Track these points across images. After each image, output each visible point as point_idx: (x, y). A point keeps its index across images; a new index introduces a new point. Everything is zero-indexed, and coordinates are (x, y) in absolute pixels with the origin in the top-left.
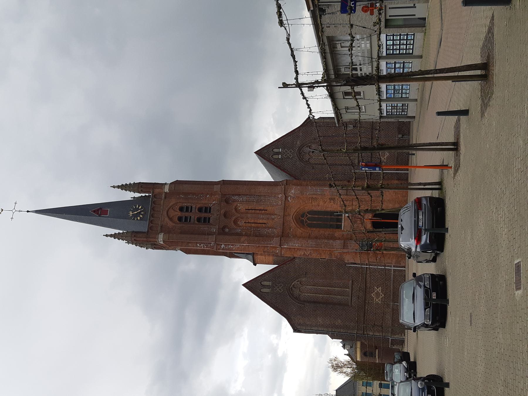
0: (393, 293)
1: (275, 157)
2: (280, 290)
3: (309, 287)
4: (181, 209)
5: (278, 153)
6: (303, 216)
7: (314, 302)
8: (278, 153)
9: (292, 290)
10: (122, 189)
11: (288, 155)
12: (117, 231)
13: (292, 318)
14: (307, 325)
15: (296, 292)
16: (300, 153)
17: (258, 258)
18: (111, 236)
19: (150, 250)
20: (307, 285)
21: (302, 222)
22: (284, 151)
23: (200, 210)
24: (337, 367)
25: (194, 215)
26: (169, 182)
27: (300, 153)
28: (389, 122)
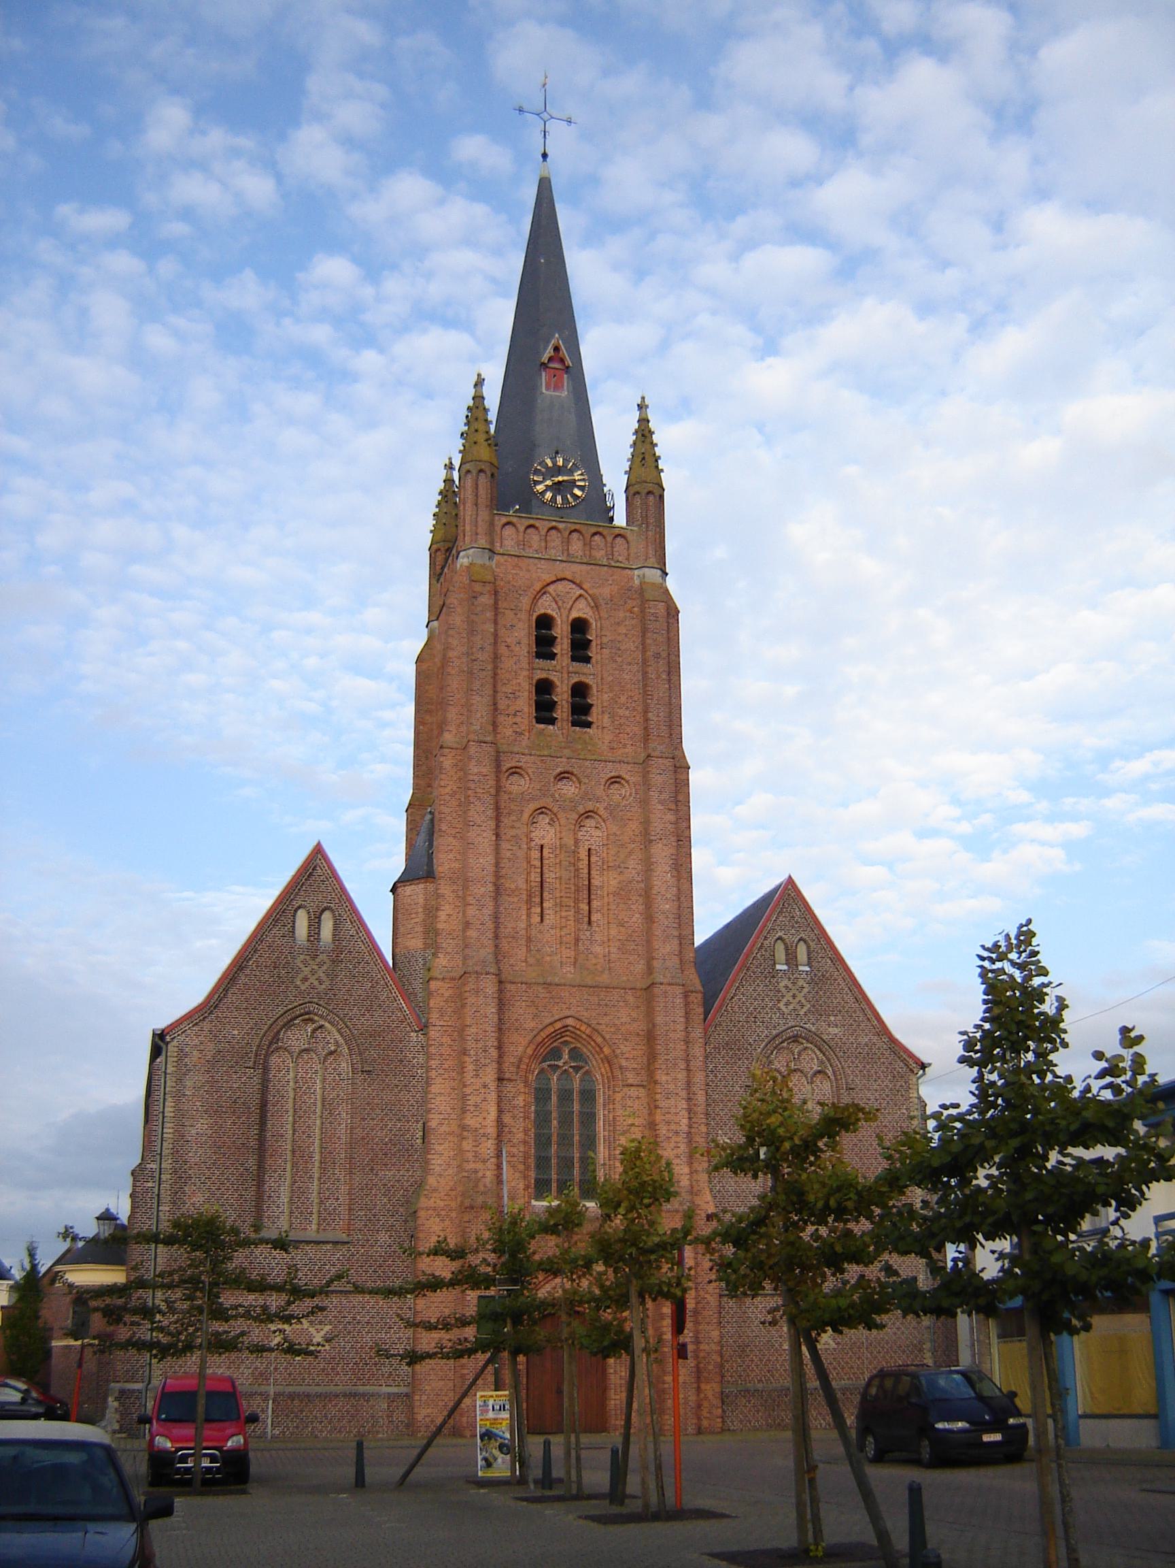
0: (308, 1396)
1: (780, 949)
2: (305, 979)
3: (319, 1085)
4: (579, 626)
5: (791, 959)
6: (575, 1054)
7: (263, 1105)
8: (791, 959)
9: (311, 1020)
10: (636, 432)
11: (788, 997)
12: (493, 416)
13: (206, 1025)
14: (179, 1081)
15: (296, 1038)
16: (795, 1039)
17: (1089, 1143)
18: (479, 398)
19: (430, 523)
20: (324, 1080)
21: (555, 1054)
22: (801, 983)
23: (580, 690)
24: (982, 1270)
25: (562, 672)
26: (671, 583)
27: (795, 1039)
28: (51, 1415)
